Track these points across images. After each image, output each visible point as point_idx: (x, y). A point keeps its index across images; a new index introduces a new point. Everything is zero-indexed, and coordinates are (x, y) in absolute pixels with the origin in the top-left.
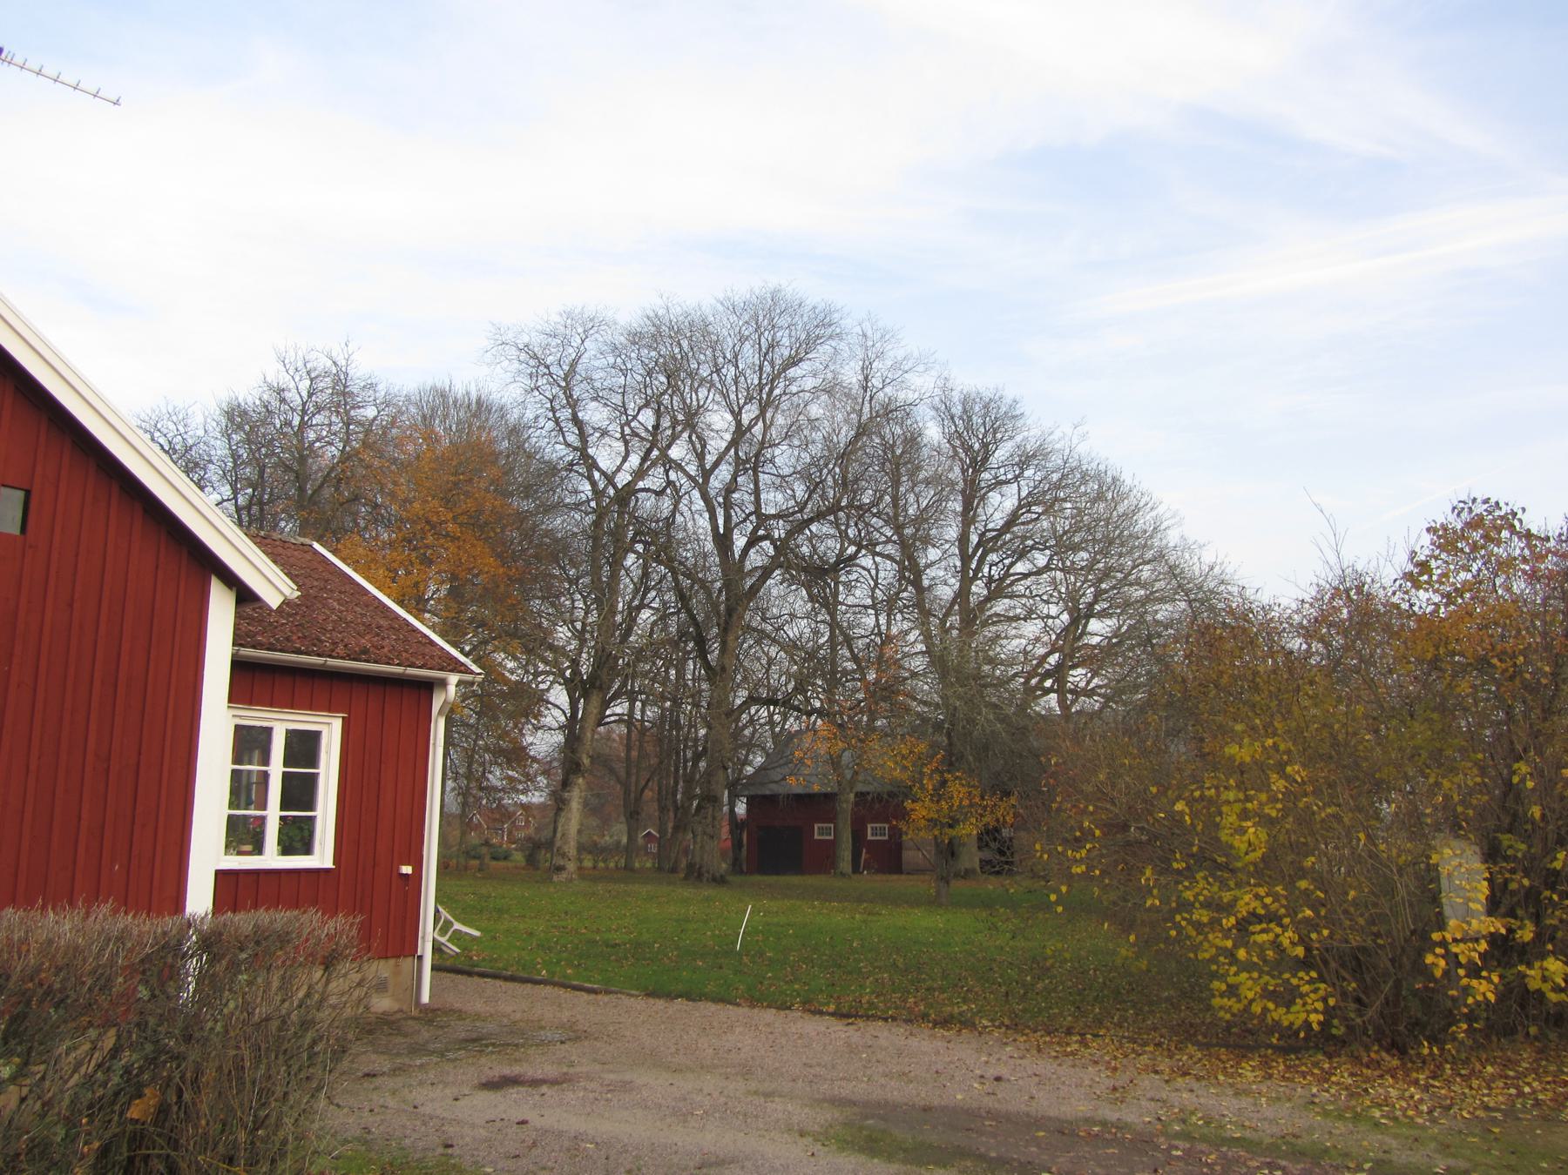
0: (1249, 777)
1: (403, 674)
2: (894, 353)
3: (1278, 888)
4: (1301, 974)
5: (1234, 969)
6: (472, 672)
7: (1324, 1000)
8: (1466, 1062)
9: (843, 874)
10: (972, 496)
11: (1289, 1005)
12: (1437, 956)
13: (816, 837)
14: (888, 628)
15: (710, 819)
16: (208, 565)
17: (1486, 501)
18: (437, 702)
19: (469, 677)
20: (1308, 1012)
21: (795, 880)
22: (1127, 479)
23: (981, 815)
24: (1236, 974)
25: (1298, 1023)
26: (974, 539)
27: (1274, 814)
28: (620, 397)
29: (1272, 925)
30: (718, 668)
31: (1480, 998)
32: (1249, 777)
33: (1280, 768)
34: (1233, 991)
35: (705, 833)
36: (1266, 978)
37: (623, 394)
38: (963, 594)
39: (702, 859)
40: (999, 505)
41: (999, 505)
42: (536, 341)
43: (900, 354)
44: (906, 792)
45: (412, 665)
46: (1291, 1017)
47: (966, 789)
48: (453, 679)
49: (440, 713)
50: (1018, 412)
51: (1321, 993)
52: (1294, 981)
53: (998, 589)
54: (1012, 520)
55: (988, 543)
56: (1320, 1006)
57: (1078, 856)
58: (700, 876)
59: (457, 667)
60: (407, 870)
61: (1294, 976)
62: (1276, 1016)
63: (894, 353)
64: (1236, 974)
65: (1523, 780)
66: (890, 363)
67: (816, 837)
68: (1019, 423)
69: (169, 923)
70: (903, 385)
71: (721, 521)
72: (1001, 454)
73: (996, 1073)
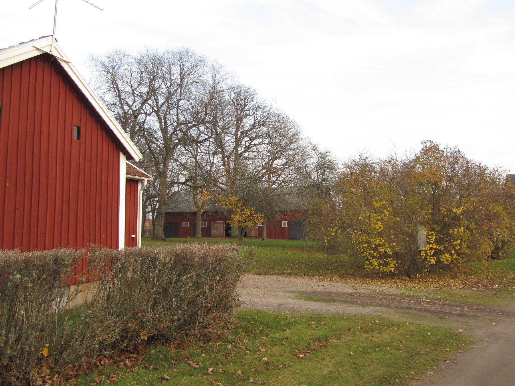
0: (379, 211)
1: (134, 178)
2: (223, 72)
3: (385, 238)
4: (388, 259)
5: (371, 258)
6: (150, 178)
7: (395, 265)
8: (425, 279)
9: (198, 238)
10: (239, 119)
11: (386, 266)
12: (424, 253)
13: (183, 226)
14: (213, 160)
15: (160, 220)
16: (120, 148)
17: (430, 141)
18: (140, 186)
19: (150, 179)
20: (391, 268)
21: (177, 239)
22: (291, 118)
23: (254, 219)
24: (372, 259)
25: (388, 271)
26: (239, 134)
27: (386, 220)
28: (129, 80)
29: (383, 247)
30: (163, 172)
31: (432, 263)
32: (379, 211)
33: (386, 209)
34: (371, 264)
35: (158, 225)
36: (379, 260)
37: (131, 79)
38: (236, 148)
39: (158, 232)
40: (247, 123)
41: (247, 123)
42: (104, 60)
43: (224, 73)
44: (231, 212)
45: (136, 175)
46: (387, 269)
47: (250, 212)
48: (146, 179)
49: (141, 189)
50: (255, 93)
51: (394, 263)
52: (387, 261)
53: (247, 149)
54: (253, 126)
55: (246, 133)
56: (393, 266)
57: (333, 230)
58: (157, 238)
59: (146, 176)
60: (133, 236)
61: (387, 259)
62: (382, 269)
63: (223, 72)
64: (372, 259)
65: (444, 212)
66: (221, 75)
67: (183, 226)
68: (255, 96)
69: (114, 251)
70: (203, 76)
71: (163, 124)
72: (251, 104)
73: (322, 284)
